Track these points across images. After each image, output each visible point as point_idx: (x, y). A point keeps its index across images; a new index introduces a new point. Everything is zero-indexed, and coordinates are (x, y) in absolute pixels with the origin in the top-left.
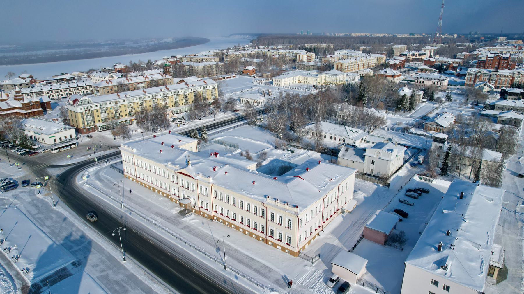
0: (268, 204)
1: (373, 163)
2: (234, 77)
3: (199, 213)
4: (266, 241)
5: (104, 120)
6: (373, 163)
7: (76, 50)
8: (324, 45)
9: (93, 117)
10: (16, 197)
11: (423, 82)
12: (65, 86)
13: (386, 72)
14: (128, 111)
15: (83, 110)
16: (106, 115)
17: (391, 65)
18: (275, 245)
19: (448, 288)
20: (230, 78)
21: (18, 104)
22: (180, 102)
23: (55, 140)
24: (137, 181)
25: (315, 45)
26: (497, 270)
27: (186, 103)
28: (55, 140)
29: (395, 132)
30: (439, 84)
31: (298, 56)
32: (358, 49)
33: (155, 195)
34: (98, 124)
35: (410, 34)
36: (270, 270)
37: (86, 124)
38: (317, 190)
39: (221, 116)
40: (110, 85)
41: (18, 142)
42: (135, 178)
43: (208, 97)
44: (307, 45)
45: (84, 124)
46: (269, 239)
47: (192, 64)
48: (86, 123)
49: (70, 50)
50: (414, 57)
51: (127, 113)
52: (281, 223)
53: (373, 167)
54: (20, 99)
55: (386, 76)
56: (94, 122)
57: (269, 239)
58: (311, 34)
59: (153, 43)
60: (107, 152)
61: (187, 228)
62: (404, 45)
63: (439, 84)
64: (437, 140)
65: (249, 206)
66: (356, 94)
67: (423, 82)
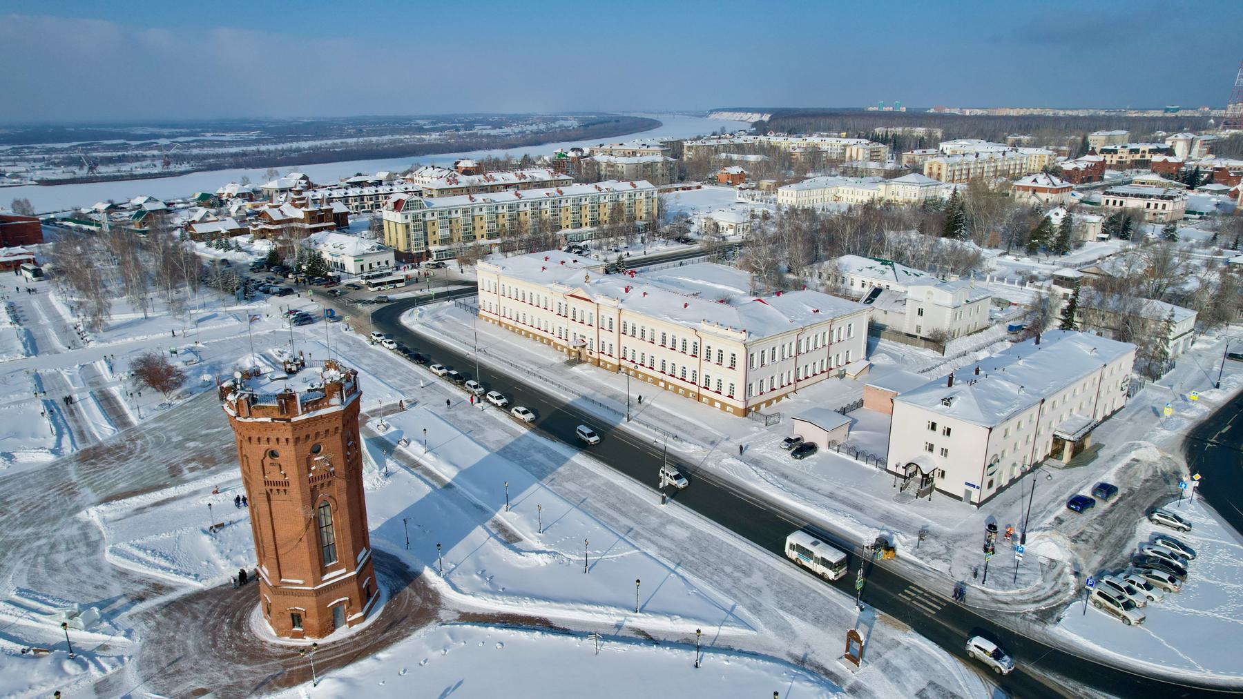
0: (703, 331)
1: (921, 313)
2: (699, 187)
3: (598, 363)
4: (699, 397)
5: (444, 241)
6: (921, 313)
7: (374, 139)
8: (920, 131)
9: (426, 234)
10: (316, 332)
11: (1121, 203)
12: (367, 191)
13: (1035, 181)
14: (486, 228)
15: (410, 220)
16: (447, 232)
17: (1067, 172)
18: (712, 402)
19: (949, 432)
20: (689, 188)
21: (300, 213)
22: (584, 221)
23: (362, 267)
24: (500, 323)
25: (899, 130)
26: (1068, 446)
27: (595, 222)
28: (362, 267)
29: (1005, 283)
30: (1160, 207)
31: (848, 150)
32: (1004, 140)
33: (529, 342)
34: (432, 248)
35: (1167, 110)
36: (697, 428)
37: (413, 246)
38: (788, 320)
39: (660, 248)
40: (454, 186)
41: (304, 267)
42: (497, 318)
43: (638, 214)
44: (879, 131)
45: (409, 245)
46: (703, 392)
47: (612, 159)
48: (413, 242)
49: (361, 139)
50: (1138, 157)
51: (485, 231)
52: (720, 362)
53: (919, 321)
54: (302, 205)
55: (1035, 191)
56: (427, 243)
57: (703, 392)
58: (904, 109)
59: (534, 127)
60: (444, 289)
61: (576, 378)
62: (1124, 132)
63: (1160, 207)
64: (1061, 281)
65: (674, 342)
66: (950, 220)
67: (1121, 203)
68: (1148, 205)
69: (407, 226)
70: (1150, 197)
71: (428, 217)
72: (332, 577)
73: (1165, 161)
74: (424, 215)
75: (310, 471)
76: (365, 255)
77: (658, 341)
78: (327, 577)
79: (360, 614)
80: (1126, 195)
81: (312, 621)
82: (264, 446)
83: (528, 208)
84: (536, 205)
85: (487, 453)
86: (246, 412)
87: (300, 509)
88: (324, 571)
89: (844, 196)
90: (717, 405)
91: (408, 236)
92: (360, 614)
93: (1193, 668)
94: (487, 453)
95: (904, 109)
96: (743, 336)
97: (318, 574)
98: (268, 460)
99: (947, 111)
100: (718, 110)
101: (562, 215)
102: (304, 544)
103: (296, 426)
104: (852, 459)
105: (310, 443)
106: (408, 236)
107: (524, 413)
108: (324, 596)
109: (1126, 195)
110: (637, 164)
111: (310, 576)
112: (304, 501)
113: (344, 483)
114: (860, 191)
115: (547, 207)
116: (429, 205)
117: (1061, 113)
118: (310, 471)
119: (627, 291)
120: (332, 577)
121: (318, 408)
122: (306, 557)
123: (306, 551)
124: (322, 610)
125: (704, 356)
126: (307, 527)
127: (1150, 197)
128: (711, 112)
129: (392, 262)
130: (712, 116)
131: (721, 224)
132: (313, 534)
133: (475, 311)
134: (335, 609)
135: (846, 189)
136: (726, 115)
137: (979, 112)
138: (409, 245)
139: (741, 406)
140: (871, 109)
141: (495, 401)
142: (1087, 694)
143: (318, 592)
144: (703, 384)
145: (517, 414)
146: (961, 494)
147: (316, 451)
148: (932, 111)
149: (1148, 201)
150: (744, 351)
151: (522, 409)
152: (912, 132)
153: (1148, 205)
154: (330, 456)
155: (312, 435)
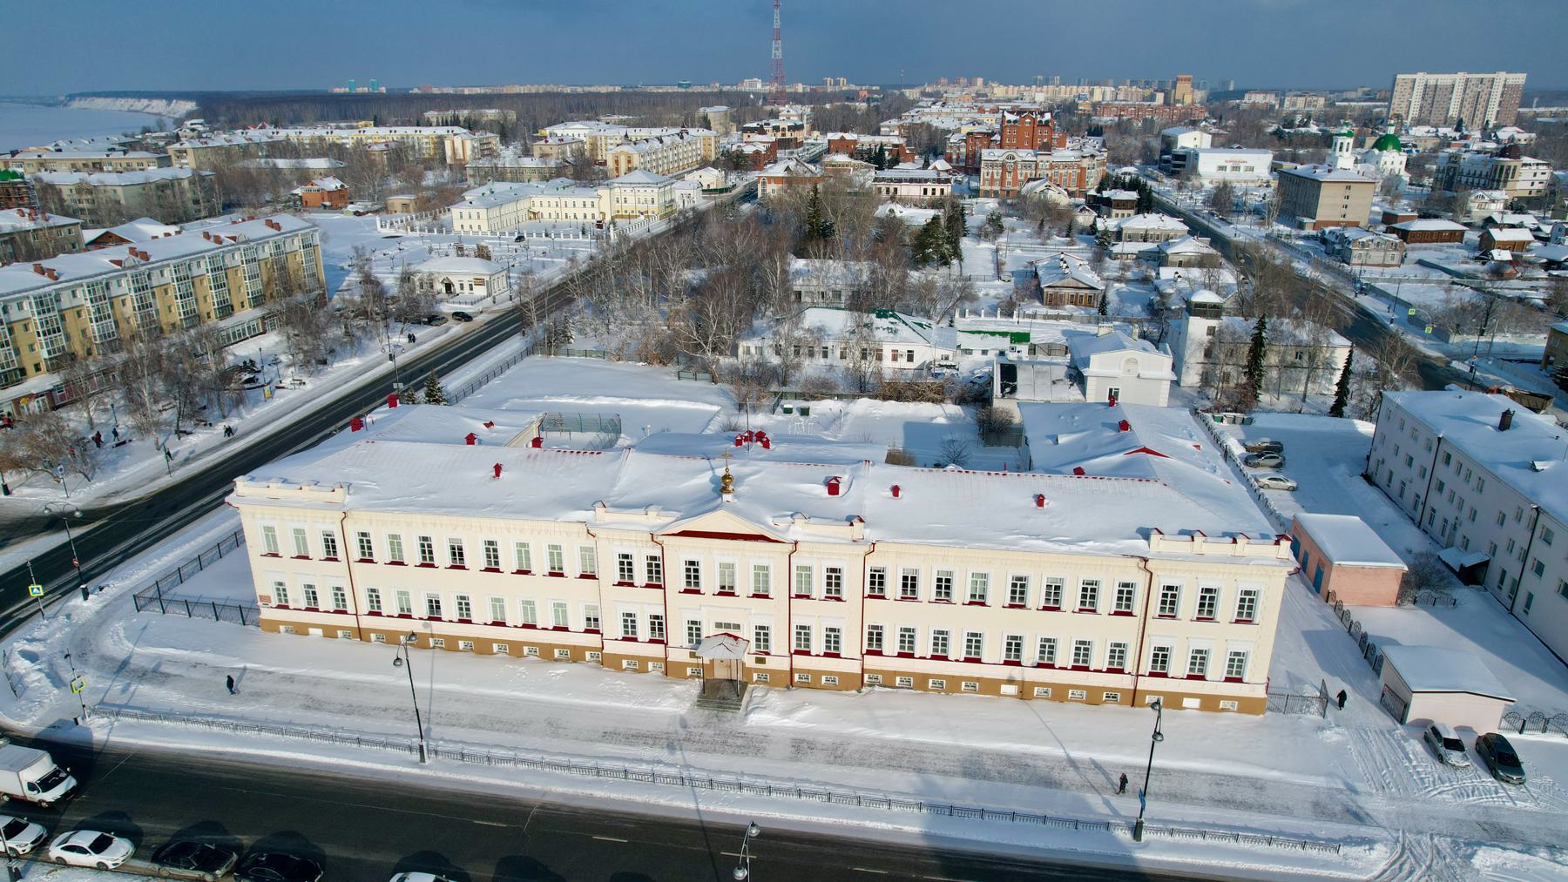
18: (301, 629)
31: (448, 144)
62: (724, 108)
68: (925, 191)
70: (926, 181)
73: (843, 139)
77: (413, 555)
80: (900, 181)
83: (83, 298)
84: (101, 292)
89: (545, 211)
95: (383, 90)
99: (436, 91)
100: (84, 95)
101: (158, 303)
107: (99, 846)
109: (900, 181)
110: (144, 185)
114: (570, 201)
115: (124, 288)
117: (579, 90)
119: (833, 489)
125: (356, 553)
127: (926, 181)
128: (72, 97)
130: (77, 104)
131: (455, 281)
135: (545, 200)
136: (100, 103)
137: (479, 91)
140: (337, 90)
141: (92, 859)
144: (365, 607)
145: (71, 857)
148: (416, 91)
149: (924, 186)
151: (86, 838)
152: (481, 115)
153: (925, 191)
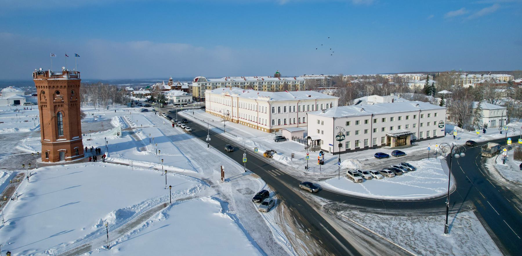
15: (200, 86)
38: (294, 97)
45: (199, 95)
48: (201, 94)
69: (199, 88)
71: (208, 85)
72: (60, 140)
74: (206, 84)
75: (54, 99)
76: (180, 96)
78: (58, 140)
79: (70, 157)
81: (51, 155)
82: (41, 89)
85: (163, 135)
86: (35, 77)
87: (49, 112)
88: (57, 138)
90: (262, 129)
91: (199, 91)
92: (70, 157)
93: (367, 193)
94: (163, 135)
96: (268, 99)
97: (55, 138)
98: (42, 95)
102: (50, 126)
103: (49, 82)
104: (298, 143)
105: (55, 90)
106: (199, 91)
108: (57, 147)
111: (52, 138)
112: (51, 110)
113: (67, 107)
116: (208, 81)
118: (54, 99)
120: (60, 140)
121: (58, 78)
122: (51, 130)
123: (51, 128)
124: (55, 152)
126: (52, 119)
129: (191, 100)
132: (54, 123)
133: (204, 108)
134: (60, 153)
138: (199, 95)
139: (268, 128)
142: (395, 255)
143: (54, 145)
146: (328, 150)
147: (58, 93)
150: (269, 105)
154: (62, 95)
155: (56, 86)
